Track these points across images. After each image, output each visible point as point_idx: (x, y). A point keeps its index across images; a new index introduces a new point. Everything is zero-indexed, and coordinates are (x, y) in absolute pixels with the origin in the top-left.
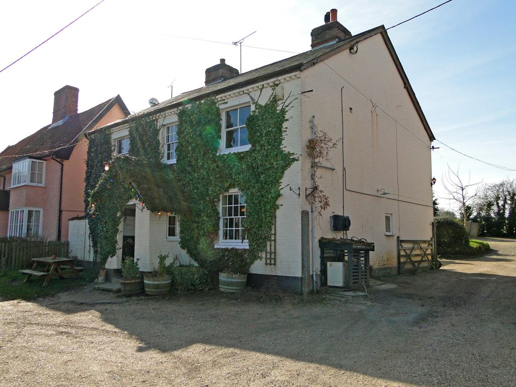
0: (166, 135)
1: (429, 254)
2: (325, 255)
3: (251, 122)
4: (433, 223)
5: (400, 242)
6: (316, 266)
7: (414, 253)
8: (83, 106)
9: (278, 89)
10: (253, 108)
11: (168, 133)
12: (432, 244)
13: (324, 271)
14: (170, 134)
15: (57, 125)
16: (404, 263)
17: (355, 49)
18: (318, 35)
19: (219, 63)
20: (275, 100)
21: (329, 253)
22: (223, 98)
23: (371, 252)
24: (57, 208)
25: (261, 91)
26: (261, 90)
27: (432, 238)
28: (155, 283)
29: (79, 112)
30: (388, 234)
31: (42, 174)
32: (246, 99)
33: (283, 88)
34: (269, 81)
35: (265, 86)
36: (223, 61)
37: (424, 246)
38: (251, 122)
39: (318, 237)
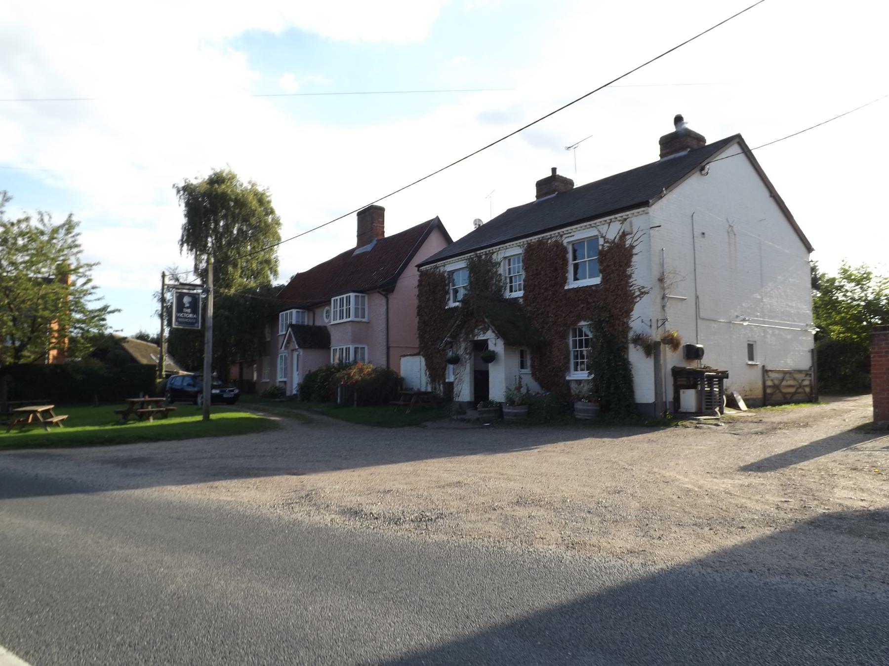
0: (507, 267)
1: (806, 386)
2: (679, 383)
3: (603, 256)
4: (812, 350)
5: (765, 371)
6: (670, 397)
7: (784, 383)
8: (392, 227)
9: (627, 223)
10: (601, 241)
11: (509, 265)
12: (810, 375)
13: (677, 398)
14: (512, 266)
15: (363, 251)
16: (772, 394)
17: (706, 170)
18: (667, 143)
19: (550, 174)
20: (624, 235)
21: (683, 381)
22: (570, 231)
23: (725, 380)
24: (385, 344)
25: (609, 225)
26: (609, 224)
27: (811, 367)
28: (515, 411)
29: (387, 235)
30: (750, 363)
31: (364, 309)
32: (592, 232)
33: (631, 223)
34: (617, 216)
35: (613, 220)
36: (554, 170)
37: (798, 376)
38: (603, 256)
39: (669, 367)
